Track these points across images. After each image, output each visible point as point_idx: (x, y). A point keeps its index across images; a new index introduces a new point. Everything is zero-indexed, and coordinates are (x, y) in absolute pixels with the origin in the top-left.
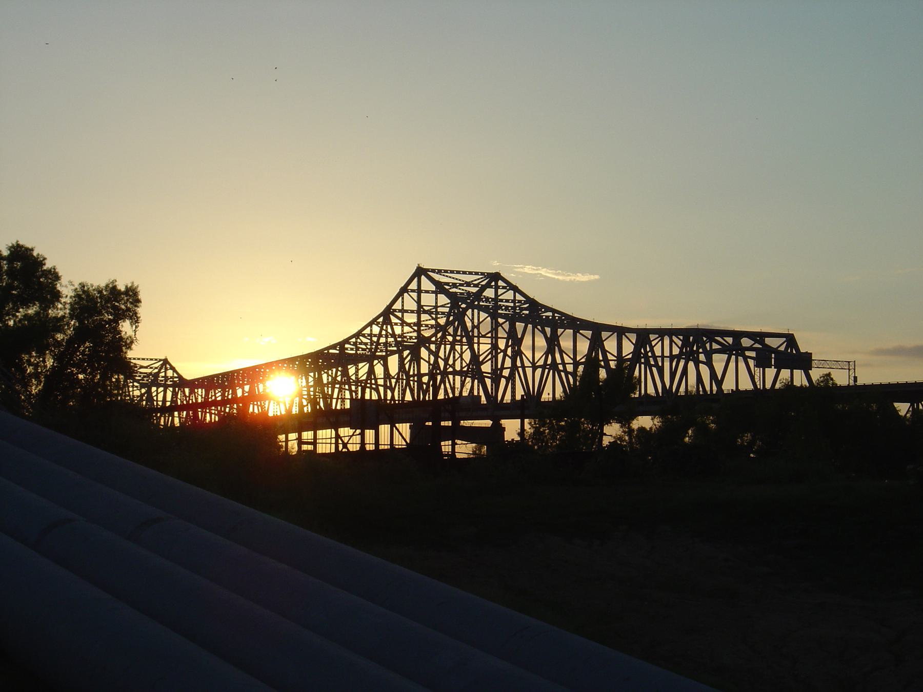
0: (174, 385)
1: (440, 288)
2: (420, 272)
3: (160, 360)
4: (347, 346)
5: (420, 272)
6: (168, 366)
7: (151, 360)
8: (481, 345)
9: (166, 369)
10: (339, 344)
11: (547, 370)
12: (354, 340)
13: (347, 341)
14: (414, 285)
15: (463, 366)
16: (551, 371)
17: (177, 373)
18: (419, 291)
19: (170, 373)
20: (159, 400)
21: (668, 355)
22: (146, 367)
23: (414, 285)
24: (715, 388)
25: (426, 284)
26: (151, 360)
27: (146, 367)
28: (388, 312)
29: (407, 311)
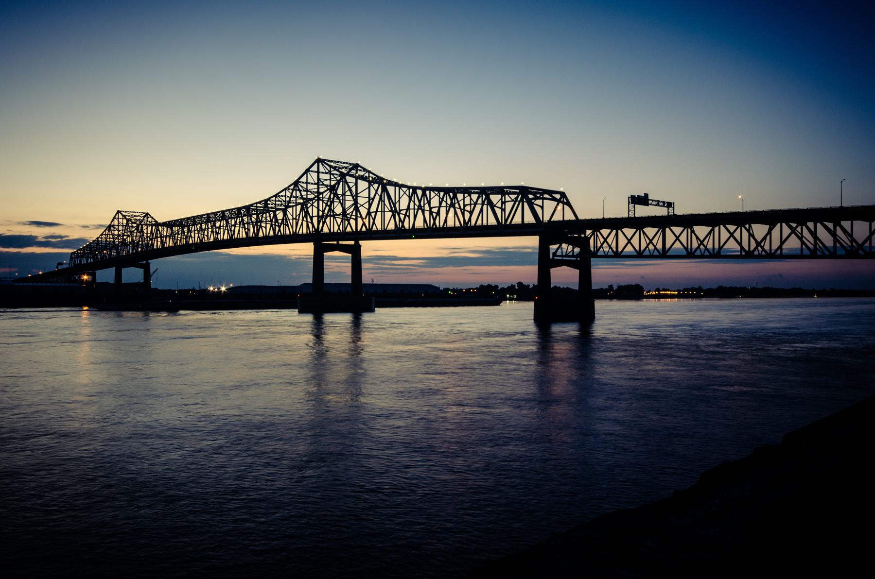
0: (152, 225)
1: (124, 217)
2: (118, 212)
3: (144, 213)
4: (269, 202)
5: (118, 212)
6: (149, 216)
7: (140, 213)
8: (368, 196)
9: (148, 218)
10: (264, 200)
11: (517, 203)
12: (274, 198)
13: (269, 199)
14: (315, 168)
15: (146, 230)
16: (521, 203)
17: (154, 219)
18: (318, 172)
19: (150, 219)
20: (413, 210)
21: (316, 215)
22: (138, 216)
23: (117, 217)
24: (401, 224)
25: (120, 216)
26: (140, 213)
27: (138, 216)
28: (296, 183)
29: (309, 183)
